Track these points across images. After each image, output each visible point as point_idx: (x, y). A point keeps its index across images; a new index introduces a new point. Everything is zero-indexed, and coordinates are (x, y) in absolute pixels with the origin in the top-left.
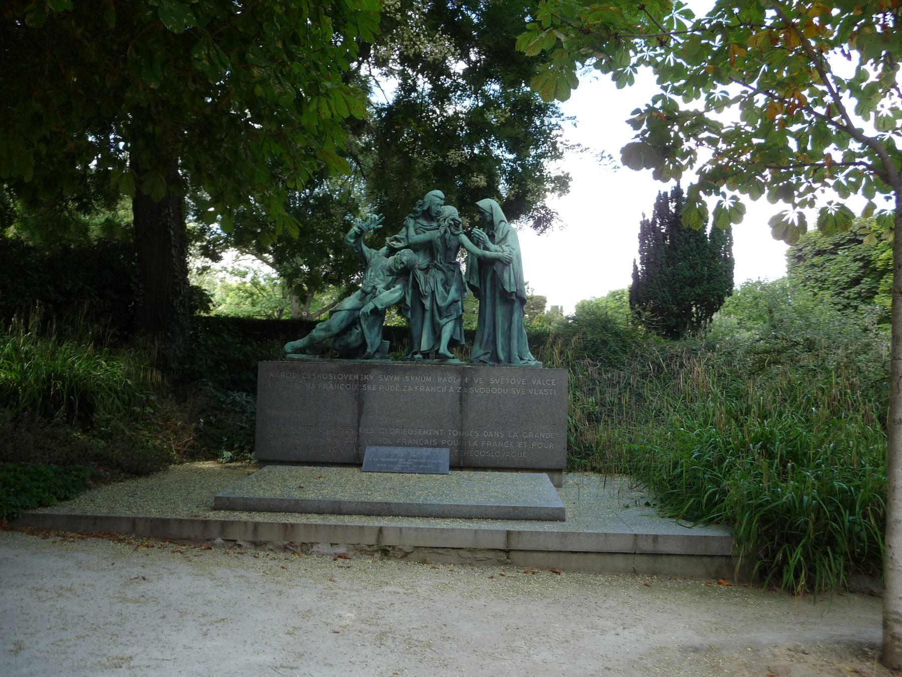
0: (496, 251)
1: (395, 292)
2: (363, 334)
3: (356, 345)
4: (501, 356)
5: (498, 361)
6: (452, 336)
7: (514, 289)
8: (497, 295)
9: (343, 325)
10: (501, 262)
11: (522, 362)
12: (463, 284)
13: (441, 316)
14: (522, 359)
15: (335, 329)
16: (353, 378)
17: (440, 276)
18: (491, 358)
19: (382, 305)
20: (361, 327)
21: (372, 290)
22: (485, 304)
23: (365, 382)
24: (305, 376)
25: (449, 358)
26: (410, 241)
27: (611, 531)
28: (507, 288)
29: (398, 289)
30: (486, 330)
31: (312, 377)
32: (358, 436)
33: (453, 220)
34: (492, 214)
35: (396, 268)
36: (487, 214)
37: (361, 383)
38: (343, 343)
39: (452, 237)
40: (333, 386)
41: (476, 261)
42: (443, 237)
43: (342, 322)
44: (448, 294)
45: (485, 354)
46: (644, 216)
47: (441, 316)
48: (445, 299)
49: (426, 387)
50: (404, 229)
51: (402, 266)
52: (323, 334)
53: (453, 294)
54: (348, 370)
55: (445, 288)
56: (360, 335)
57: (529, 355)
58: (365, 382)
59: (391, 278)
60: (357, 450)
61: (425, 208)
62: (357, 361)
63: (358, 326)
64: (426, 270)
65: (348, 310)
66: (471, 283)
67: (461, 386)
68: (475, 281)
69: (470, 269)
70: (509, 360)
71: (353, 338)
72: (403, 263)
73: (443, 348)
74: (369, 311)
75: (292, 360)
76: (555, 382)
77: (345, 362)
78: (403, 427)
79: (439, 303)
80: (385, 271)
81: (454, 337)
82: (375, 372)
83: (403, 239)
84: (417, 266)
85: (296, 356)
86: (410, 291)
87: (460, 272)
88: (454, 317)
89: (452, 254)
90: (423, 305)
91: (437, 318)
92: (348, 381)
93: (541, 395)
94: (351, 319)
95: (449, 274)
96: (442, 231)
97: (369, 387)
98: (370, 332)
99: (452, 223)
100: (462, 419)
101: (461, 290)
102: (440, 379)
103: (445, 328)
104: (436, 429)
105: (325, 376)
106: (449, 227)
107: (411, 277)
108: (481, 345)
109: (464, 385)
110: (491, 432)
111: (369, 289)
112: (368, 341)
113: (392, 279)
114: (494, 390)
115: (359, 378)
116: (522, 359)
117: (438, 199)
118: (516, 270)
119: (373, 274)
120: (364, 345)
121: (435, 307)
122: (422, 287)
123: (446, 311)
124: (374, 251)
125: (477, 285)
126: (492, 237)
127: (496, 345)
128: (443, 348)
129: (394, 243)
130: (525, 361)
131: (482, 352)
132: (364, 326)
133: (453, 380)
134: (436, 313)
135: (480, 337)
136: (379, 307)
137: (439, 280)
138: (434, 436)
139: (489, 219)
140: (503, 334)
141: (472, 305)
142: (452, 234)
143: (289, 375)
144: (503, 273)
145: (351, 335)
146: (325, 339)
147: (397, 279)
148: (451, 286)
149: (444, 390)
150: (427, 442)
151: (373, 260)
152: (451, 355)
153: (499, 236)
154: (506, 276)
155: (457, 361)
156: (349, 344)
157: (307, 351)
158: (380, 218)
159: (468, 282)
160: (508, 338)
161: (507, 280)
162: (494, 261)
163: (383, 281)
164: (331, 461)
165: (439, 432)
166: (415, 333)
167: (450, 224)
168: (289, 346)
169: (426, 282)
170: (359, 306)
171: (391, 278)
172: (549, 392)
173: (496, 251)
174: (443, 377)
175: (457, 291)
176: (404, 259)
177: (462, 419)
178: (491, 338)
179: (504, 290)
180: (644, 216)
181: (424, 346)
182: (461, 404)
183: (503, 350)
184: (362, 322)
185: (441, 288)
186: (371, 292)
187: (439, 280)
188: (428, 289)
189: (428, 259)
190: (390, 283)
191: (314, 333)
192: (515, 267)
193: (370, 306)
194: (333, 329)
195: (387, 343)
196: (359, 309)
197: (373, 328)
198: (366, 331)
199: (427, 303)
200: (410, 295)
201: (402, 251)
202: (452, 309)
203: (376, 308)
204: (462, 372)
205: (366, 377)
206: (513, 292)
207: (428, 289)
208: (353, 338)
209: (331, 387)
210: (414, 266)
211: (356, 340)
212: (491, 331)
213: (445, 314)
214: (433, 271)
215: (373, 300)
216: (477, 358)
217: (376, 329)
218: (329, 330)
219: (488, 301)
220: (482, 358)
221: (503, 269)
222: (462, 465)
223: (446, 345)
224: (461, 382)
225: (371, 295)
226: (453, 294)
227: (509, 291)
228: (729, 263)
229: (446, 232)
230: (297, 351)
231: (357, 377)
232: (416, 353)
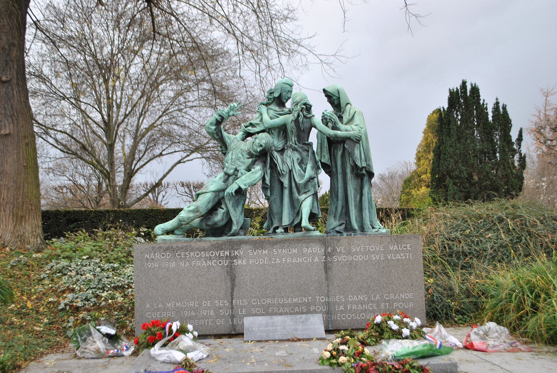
0: (346, 131)
1: (256, 172)
2: (228, 212)
4: (355, 226)
5: (354, 230)
6: (311, 210)
7: (364, 165)
8: (348, 170)
9: (210, 206)
10: (352, 140)
11: (374, 230)
12: (316, 162)
13: (299, 192)
14: (373, 228)
17: (296, 156)
19: (245, 185)
20: (227, 207)
21: (234, 172)
22: (337, 180)
23: (236, 257)
24: (179, 255)
27: (261, 318)
29: (259, 170)
31: (185, 255)
32: (232, 308)
34: (339, 98)
36: (335, 98)
37: (232, 258)
38: (210, 223)
39: (305, 120)
40: (206, 262)
41: (326, 141)
42: (296, 121)
43: (209, 203)
44: (305, 172)
45: (341, 225)
48: (302, 177)
49: (292, 258)
51: (261, 148)
53: (309, 172)
54: (218, 247)
55: (301, 167)
56: (225, 214)
57: (378, 223)
58: (236, 257)
60: (232, 321)
62: (224, 238)
63: (223, 206)
65: (214, 192)
66: (323, 161)
67: (325, 255)
68: (326, 159)
69: (321, 145)
70: (362, 229)
71: (219, 217)
72: (261, 146)
73: (305, 223)
74: (233, 191)
76: (411, 247)
77: (212, 239)
78: (274, 297)
82: (244, 247)
83: (258, 124)
84: (273, 148)
86: (269, 172)
87: (314, 151)
88: (312, 192)
89: (306, 135)
90: (282, 184)
91: (296, 195)
92: (220, 257)
93: (398, 260)
94: (216, 200)
95: (305, 154)
96: (296, 115)
97: (240, 262)
98: (235, 210)
99: (304, 107)
100: (328, 286)
101: (316, 168)
102: (305, 250)
103: (304, 203)
104: (305, 297)
105: (198, 254)
106: (302, 111)
107: (269, 158)
108: (335, 217)
109: (327, 255)
110: (355, 296)
112: (234, 219)
113: (252, 161)
114: (356, 258)
116: (373, 228)
119: (234, 157)
120: (229, 222)
121: (293, 184)
122: (280, 166)
123: (305, 188)
125: (329, 163)
127: (349, 217)
128: (305, 223)
129: (250, 128)
130: (376, 230)
132: (230, 206)
133: (318, 250)
134: (295, 190)
136: (243, 187)
137: (295, 160)
138: (304, 304)
140: (356, 206)
141: (324, 179)
142: (305, 117)
143: (163, 255)
147: (256, 161)
148: (306, 164)
149: (310, 260)
150: (297, 309)
151: (233, 144)
152: (312, 228)
156: (216, 223)
157: (176, 232)
159: (320, 161)
160: (360, 209)
162: (344, 140)
163: (243, 163)
164: (208, 333)
165: (308, 300)
167: (302, 108)
168: (159, 228)
169: (283, 162)
170: (224, 187)
171: (250, 160)
172: (406, 256)
173: (346, 131)
174: (308, 248)
175: (312, 168)
176: (263, 142)
177: (328, 286)
178: (344, 210)
179: (356, 165)
181: (286, 221)
182: (326, 272)
183: (356, 220)
184: (227, 202)
185: (297, 167)
186: (234, 174)
187: (295, 160)
188: (286, 169)
189: (283, 141)
190: (250, 164)
192: (364, 144)
193: (232, 188)
194: (201, 210)
196: (224, 190)
197: (237, 207)
199: (286, 182)
202: (310, 186)
203: (240, 188)
204: (323, 242)
205: (236, 253)
206: (364, 167)
207: (286, 169)
208: (219, 217)
209: (204, 263)
210: (271, 147)
213: (302, 191)
214: (289, 152)
217: (240, 208)
218: (198, 211)
219: (340, 177)
220: (338, 229)
221: (354, 146)
222: (331, 328)
224: (325, 252)
226: (309, 172)
227: (360, 166)
229: (298, 116)
230: (169, 232)
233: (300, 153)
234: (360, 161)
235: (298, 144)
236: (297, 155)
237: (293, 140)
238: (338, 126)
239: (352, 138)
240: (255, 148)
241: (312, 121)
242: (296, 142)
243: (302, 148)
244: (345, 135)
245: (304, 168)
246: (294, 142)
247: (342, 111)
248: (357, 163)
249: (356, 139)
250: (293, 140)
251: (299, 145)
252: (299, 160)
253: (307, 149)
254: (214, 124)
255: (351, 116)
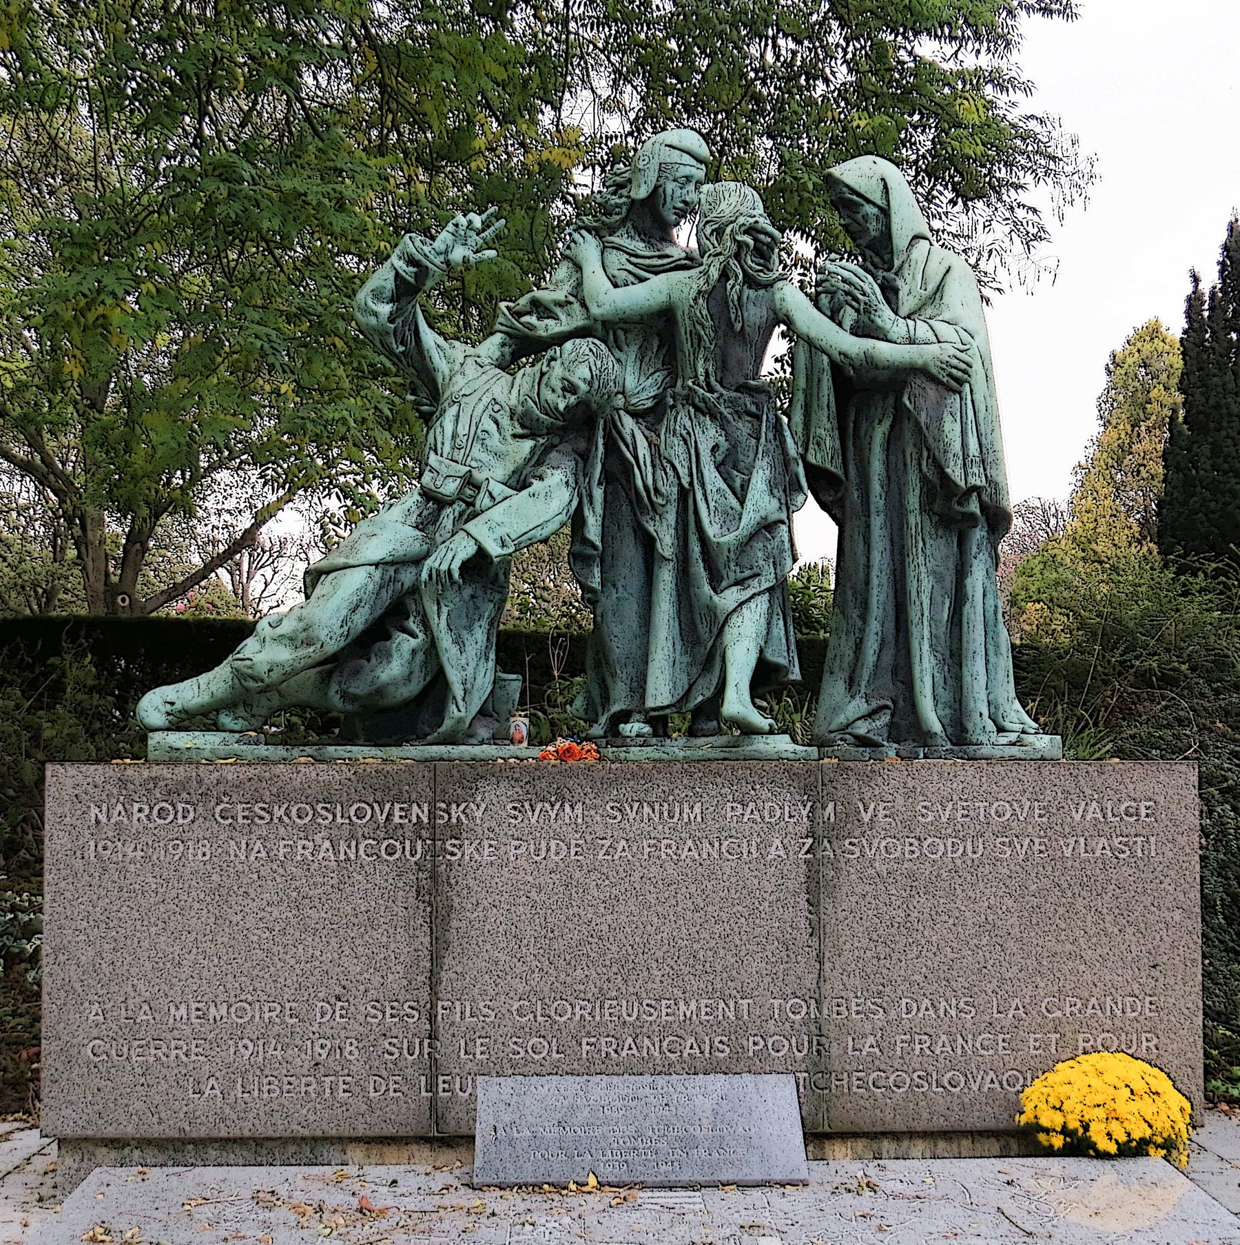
2: (432, 649)
3: (415, 687)
4: (932, 718)
5: (923, 737)
9: (360, 620)
12: (787, 462)
13: (716, 582)
15: (330, 634)
16: (406, 814)
17: (708, 436)
18: (894, 733)
25: (759, 732)
26: (595, 310)
28: (955, 472)
30: (874, 626)
32: (433, 1036)
33: (752, 230)
34: (885, 212)
35: (550, 410)
36: (870, 210)
38: (359, 687)
44: (742, 502)
45: (870, 715)
46: (1196, 280)
47: (716, 582)
48: (731, 518)
50: (563, 271)
51: (572, 399)
52: (284, 655)
55: (727, 480)
56: (420, 657)
59: (528, 444)
61: (642, 192)
64: (652, 416)
66: (811, 458)
70: (959, 734)
72: (570, 388)
75: (175, 758)
79: (712, 530)
80: (505, 421)
81: (771, 656)
85: (180, 740)
86: (598, 493)
90: (648, 543)
94: (386, 596)
95: (743, 428)
96: (714, 273)
98: (459, 642)
106: (737, 256)
108: (851, 683)
111: (450, 488)
112: (454, 676)
115: (432, 815)
117: (687, 159)
118: (981, 407)
121: (696, 549)
122: (644, 476)
124: (459, 350)
125: (835, 468)
126: (890, 293)
128: (738, 702)
129: (532, 319)
130: (1013, 737)
131: (858, 706)
134: (699, 570)
135: (849, 653)
136: (494, 550)
139: (873, 228)
142: (750, 281)
143: (162, 813)
144: (940, 419)
145: (388, 656)
146: (295, 672)
151: (459, 381)
153: (910, 291)
154: (952, 429)
155: (782, 744)
156: (380, 691)
158: (486, 225)
161: (956, 447)
166: (620, 642)
170: (416, 548)
175: (772, 487)
178: (888, 658)
180: (1196, 280)
185: (711, 476)
189: (659, 376)
190: (527, 461)
191: (250, 647)
194: (323, 635)
195: (514, 683)
196: (418, 561)
197: (470, 628)
198: (446, 642)
200: (599, 509)
201: (568, 345)
202: (758, 553)
203: (481, 553)
206: (975, 488)
211: (408, 678)
212: (890, 625)
213: (733, 573)
214: (683, 419)
215: (470, 526)
216: (844, 729)
217: (480, 634)
220: (862, 728)
221: (940, 405)
223: (746, 687)
225: (458, 507)
228: (824, 506)
229: (724, 275)
230: (183, 720)
231: (420, 813)
232: (624, 717)
233: (723, 424)
234: (960, 462)
235: (718, 387)
236: (712, 432)
237: (701, 370)
238: (879, 321)
239: (934, 371)
240: (548, 395)
241: (778, 296)
242: (712, 379)
243: (732, 403)
244: (907, 356)
245: (738, 484)
246: (702, 378)
247: (897, 263)
248: (949, 471)
249: (950, 375)
250: (701, 370)
251: (724, 392)
252: (722, 449)
253: (753, 409)
254: (388, 294)
255: (932, 286)
